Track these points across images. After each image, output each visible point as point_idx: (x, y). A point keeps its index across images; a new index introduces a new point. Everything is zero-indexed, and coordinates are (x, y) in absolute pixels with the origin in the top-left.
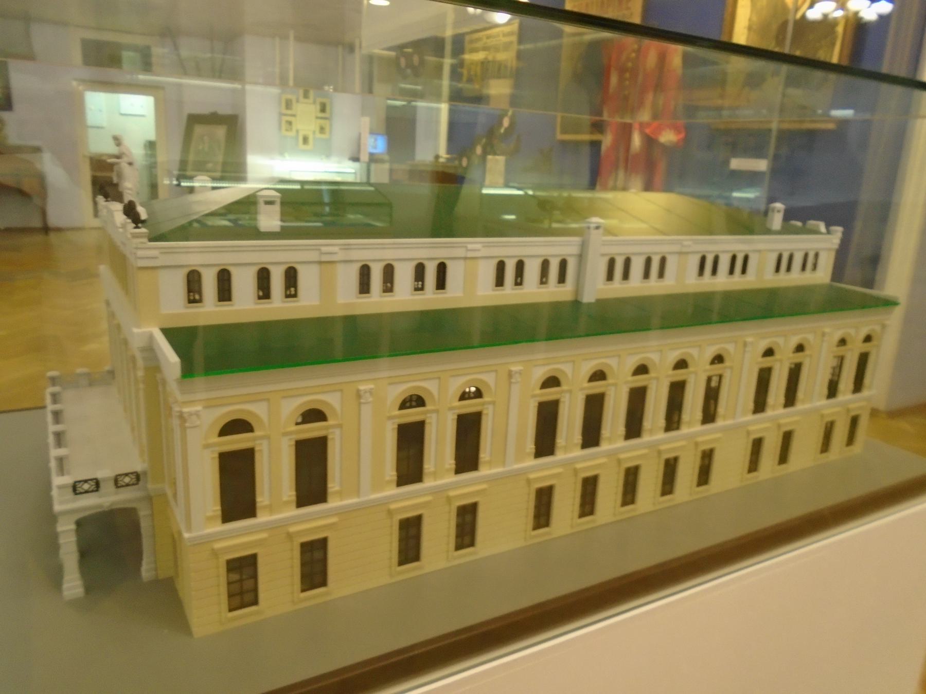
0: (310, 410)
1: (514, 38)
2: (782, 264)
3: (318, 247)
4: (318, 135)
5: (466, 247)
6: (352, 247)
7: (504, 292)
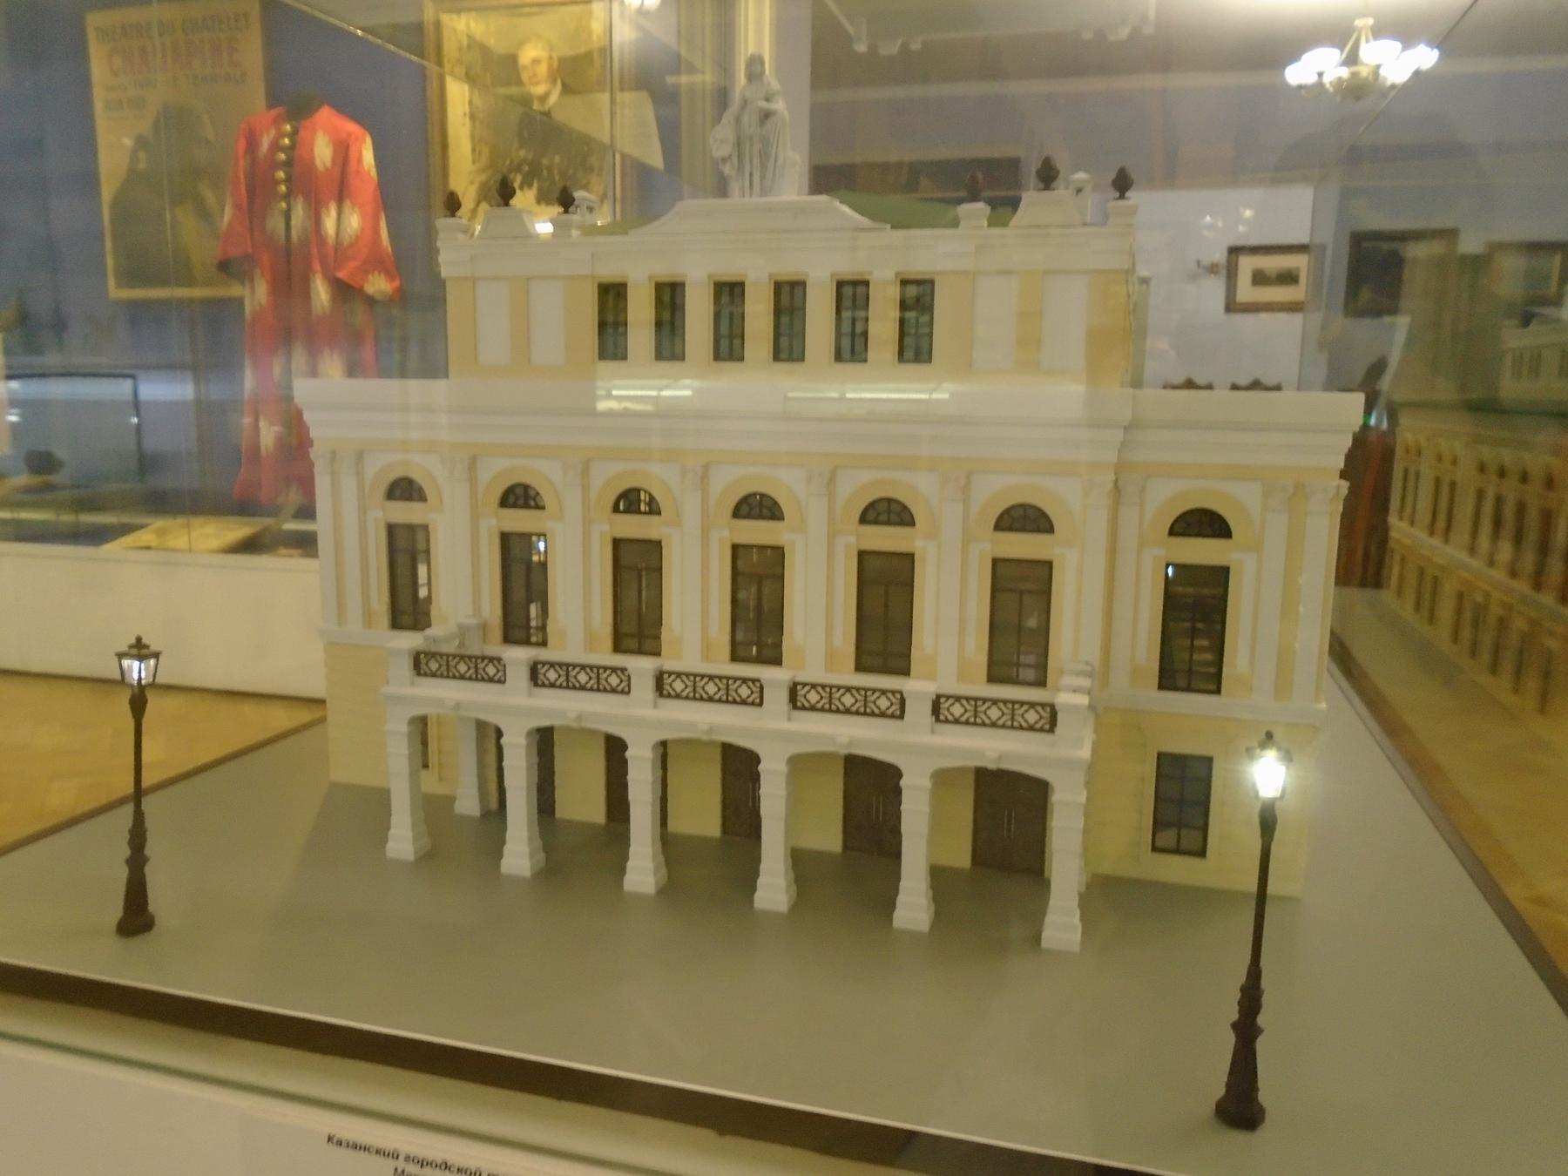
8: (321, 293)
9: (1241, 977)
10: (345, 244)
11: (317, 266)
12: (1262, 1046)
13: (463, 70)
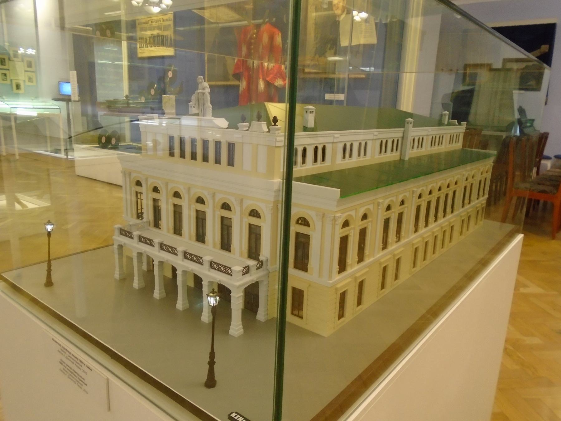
0: (176, 269)
1: (171, 23)
2: (346, 151)
3: (333, 135)
4: (28, 83)
5: (374, 134)
6: (318, 136)
7: (387, 155)
8: (262, 85)
9: (210, 350)
10: (270, 69)
11: (261, 76)
12: (216, 367)
13: (314, 7)
